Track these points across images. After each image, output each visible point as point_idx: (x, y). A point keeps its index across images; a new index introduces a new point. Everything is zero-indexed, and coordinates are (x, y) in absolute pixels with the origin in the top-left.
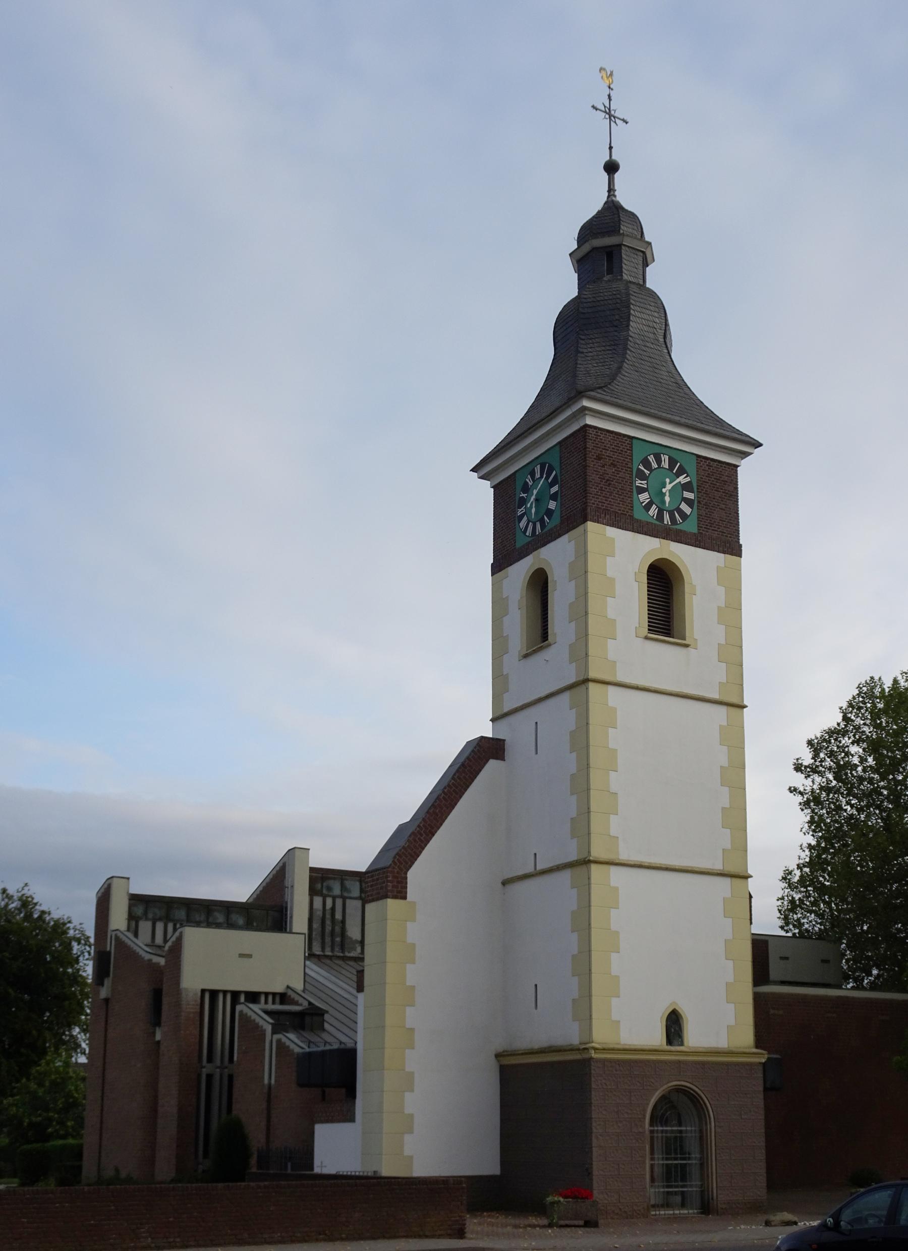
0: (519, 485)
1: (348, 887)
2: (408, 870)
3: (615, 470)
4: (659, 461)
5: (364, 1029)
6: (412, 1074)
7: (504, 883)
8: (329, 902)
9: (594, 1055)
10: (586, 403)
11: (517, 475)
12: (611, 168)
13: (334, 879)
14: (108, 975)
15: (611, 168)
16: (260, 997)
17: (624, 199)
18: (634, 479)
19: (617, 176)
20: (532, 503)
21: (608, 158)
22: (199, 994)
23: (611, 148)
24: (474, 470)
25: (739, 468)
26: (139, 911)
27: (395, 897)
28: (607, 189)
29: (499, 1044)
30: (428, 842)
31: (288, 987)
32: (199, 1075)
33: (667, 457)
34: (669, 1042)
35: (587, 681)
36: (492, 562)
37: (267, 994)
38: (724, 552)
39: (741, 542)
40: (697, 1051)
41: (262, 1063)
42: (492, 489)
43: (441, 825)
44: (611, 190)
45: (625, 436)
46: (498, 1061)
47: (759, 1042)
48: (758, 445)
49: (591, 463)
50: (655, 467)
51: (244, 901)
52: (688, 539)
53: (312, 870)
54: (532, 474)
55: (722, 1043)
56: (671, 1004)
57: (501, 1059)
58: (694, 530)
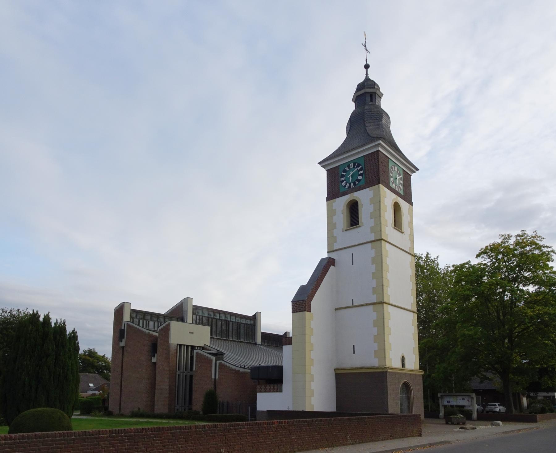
0: (341, 170)
1: (204, 312)
2: (311, 302)
5: (293, 358)
6: (313, 375)
7: (336, 309)
8: (198, 317)
9: (389, 370)
10: (381, 142)
11: (340, 166)
12: (367, 67)
13: (200, 309)
14: (124, 338)
15: (367, 67)
16: (189, 347)
17: (371, 77)
19: (369, 70)
20: (350, 177)
21: (366, 63)
22: (176, 345)
23: (366, 60)
24: (319, 163)
25: (411, 177)
26: (134, 315)
27: (308, 311)
28: (365, 74)
29: (335, 366)
31: (205, 345)
32: (176, 375)
33: (352, 164)
34: (403, 367)
35: (382, 239)
36: (327, 196)
37: (198, 347)
39: (413, 201)
41: (211, 371)
42: (326, 171)
44: (367, 74)
46: (335, 372)
47: (421, 368)
48: (418, 170)
49: (380, 164)
51: (163, 313)
53: (194, 306)
54: (349, 166)
57: (336, 371)
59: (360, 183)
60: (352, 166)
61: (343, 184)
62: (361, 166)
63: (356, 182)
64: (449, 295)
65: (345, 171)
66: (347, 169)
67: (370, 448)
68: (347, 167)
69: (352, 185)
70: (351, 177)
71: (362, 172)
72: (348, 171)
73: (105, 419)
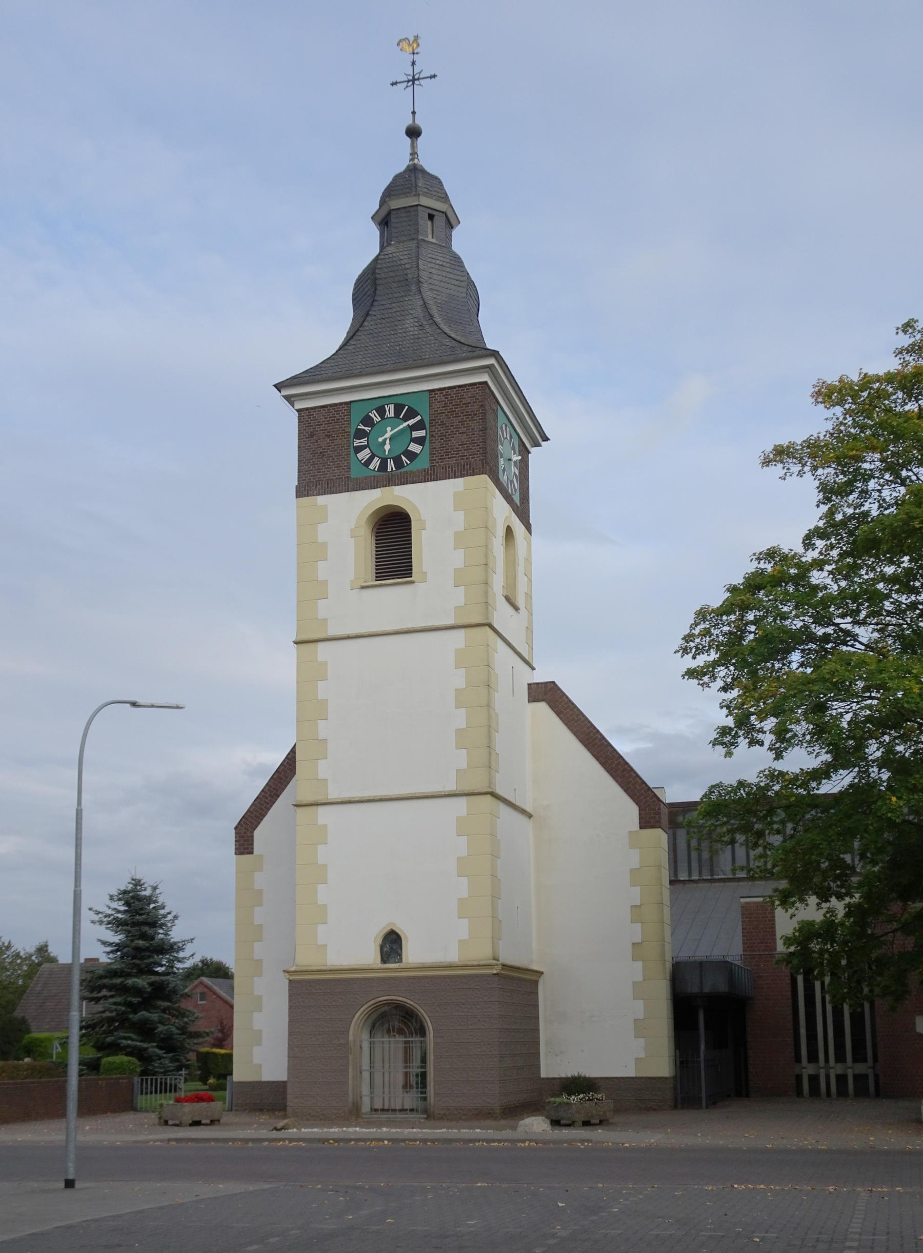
0: (356, 416)
2: (255, 829)
3: (330, 440)
4: (381, 411)
11: (352, 405)
12: (413, 133)
15: (413, 133)
17: (427, 163)
18: (352, 441)
23: (414, 113)
30: (274, 803)
33: (392, 406)
38: (462, 476)
40: (408, 967)
43: (286, 786)
44: (414, 154)
45: (341, 404)
50: (378, 421)
52: (416, 477)
54: (381, 411)
55: (452, 955)
56: (387, 925)
58: (427, 465)
59: (414, 462)
60: (390, 411)
61: (361, 455)
62: (419, 418)
63: (403, 458)
64: (712, 616)
65: (368, 421)
66: (377, 419)
67: (366, 1200)
68: (374, 411)
69: (391, 465)
70: (388, 442)
71: (421, 433)
72: (377, 422)
73: (249, 1133)
